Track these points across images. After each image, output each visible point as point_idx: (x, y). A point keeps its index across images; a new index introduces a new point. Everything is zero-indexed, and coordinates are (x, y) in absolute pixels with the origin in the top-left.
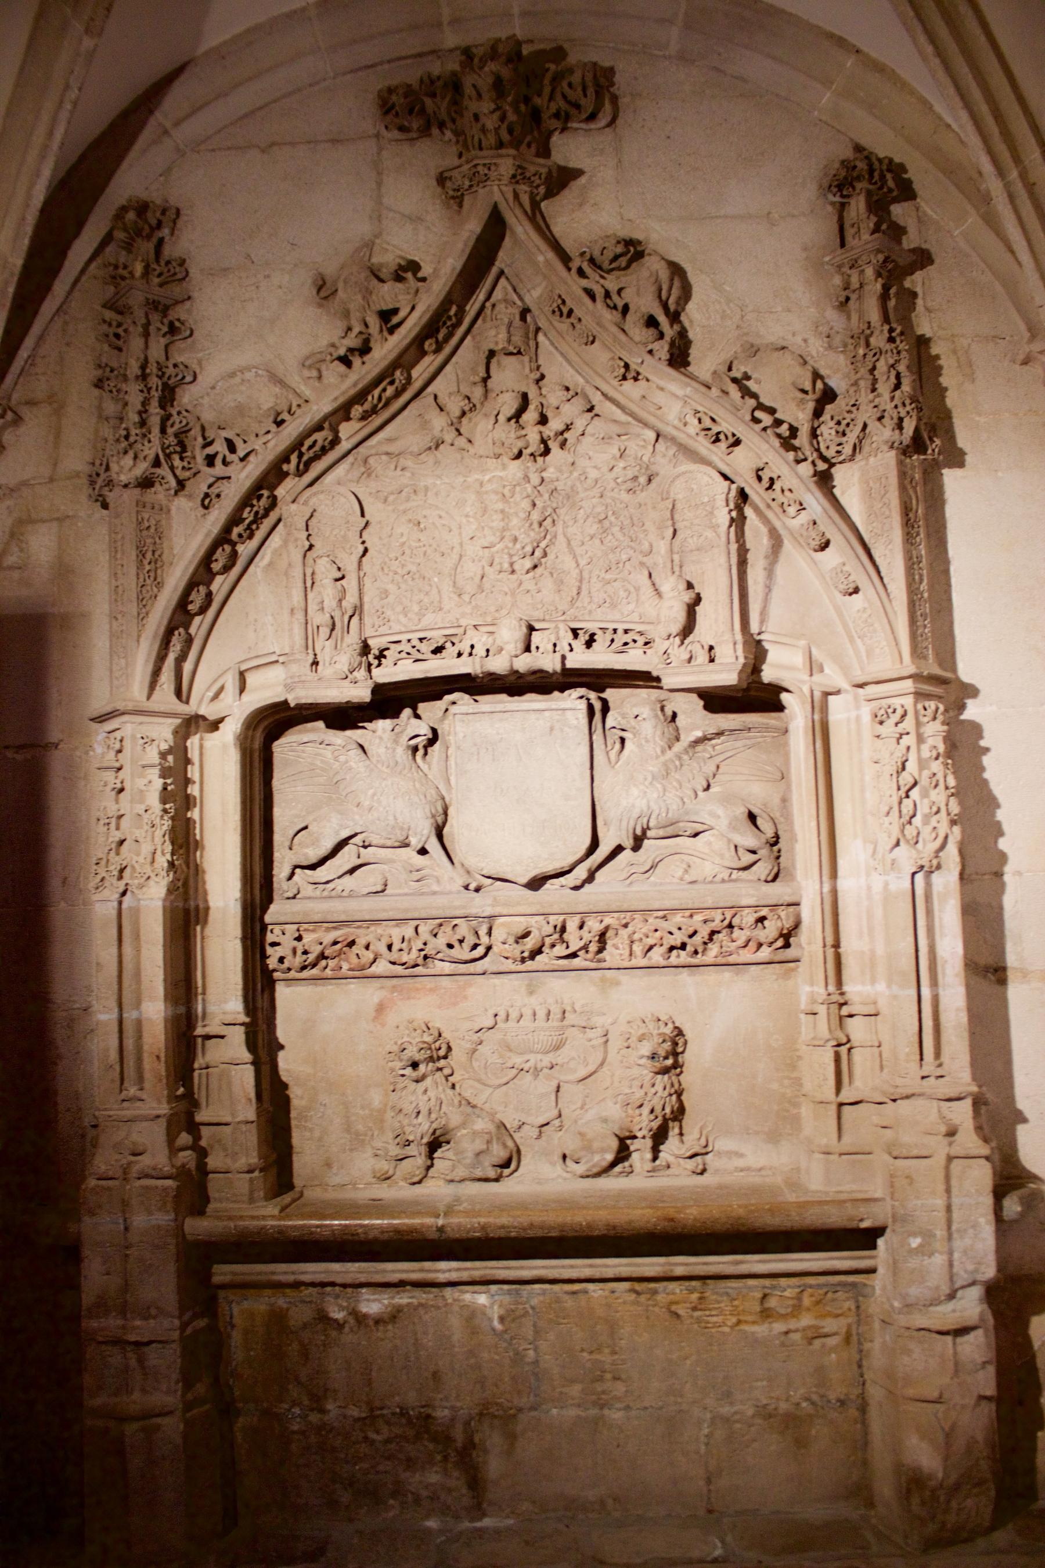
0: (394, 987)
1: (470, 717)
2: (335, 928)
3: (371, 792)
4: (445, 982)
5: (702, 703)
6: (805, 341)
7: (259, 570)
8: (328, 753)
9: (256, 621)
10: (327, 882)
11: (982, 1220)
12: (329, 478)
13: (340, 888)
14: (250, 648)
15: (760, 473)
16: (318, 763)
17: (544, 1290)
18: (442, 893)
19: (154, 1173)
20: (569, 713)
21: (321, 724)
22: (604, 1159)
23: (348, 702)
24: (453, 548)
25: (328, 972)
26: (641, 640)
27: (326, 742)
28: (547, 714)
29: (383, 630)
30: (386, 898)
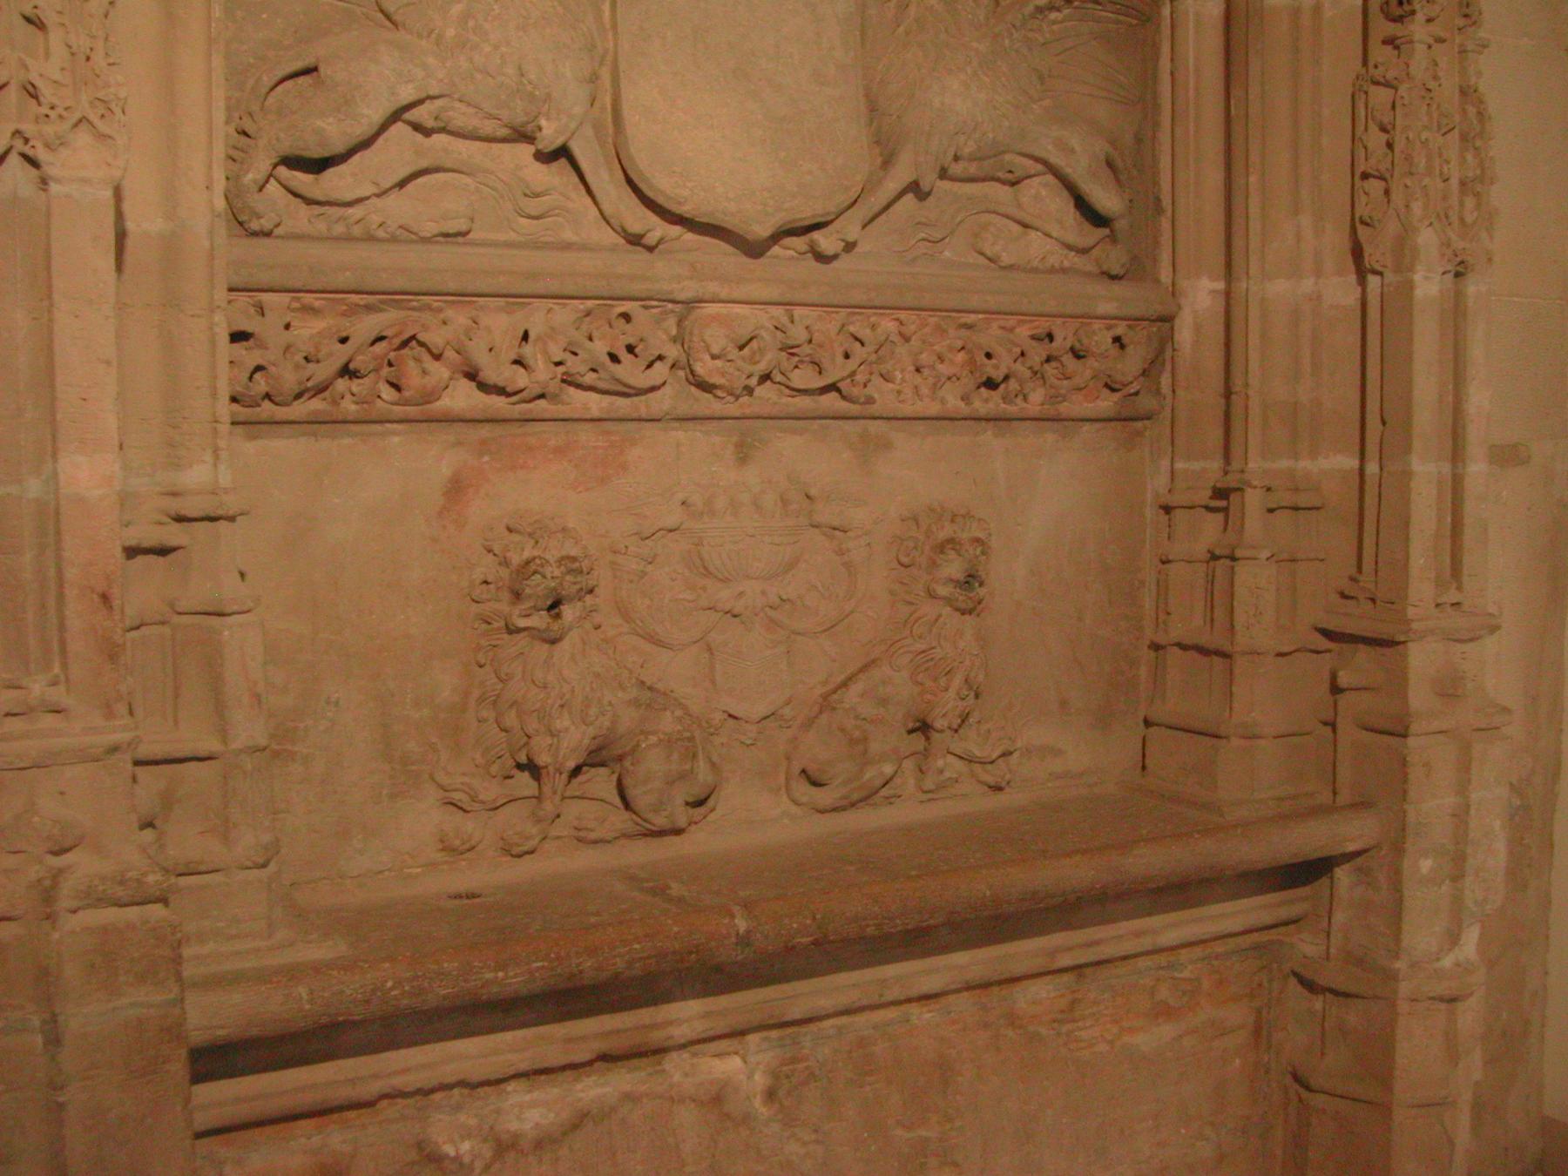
0: (483, 442)
2: (369, 308)
4: (586, 436)
10: (349, 204)
11: (1497, 824)
13: (376, 219)
17: (840, 1029)
18: (583, 247)
19: (120, 892)
22: (882, 773)
25: (349, 407)
30: (469, 249)
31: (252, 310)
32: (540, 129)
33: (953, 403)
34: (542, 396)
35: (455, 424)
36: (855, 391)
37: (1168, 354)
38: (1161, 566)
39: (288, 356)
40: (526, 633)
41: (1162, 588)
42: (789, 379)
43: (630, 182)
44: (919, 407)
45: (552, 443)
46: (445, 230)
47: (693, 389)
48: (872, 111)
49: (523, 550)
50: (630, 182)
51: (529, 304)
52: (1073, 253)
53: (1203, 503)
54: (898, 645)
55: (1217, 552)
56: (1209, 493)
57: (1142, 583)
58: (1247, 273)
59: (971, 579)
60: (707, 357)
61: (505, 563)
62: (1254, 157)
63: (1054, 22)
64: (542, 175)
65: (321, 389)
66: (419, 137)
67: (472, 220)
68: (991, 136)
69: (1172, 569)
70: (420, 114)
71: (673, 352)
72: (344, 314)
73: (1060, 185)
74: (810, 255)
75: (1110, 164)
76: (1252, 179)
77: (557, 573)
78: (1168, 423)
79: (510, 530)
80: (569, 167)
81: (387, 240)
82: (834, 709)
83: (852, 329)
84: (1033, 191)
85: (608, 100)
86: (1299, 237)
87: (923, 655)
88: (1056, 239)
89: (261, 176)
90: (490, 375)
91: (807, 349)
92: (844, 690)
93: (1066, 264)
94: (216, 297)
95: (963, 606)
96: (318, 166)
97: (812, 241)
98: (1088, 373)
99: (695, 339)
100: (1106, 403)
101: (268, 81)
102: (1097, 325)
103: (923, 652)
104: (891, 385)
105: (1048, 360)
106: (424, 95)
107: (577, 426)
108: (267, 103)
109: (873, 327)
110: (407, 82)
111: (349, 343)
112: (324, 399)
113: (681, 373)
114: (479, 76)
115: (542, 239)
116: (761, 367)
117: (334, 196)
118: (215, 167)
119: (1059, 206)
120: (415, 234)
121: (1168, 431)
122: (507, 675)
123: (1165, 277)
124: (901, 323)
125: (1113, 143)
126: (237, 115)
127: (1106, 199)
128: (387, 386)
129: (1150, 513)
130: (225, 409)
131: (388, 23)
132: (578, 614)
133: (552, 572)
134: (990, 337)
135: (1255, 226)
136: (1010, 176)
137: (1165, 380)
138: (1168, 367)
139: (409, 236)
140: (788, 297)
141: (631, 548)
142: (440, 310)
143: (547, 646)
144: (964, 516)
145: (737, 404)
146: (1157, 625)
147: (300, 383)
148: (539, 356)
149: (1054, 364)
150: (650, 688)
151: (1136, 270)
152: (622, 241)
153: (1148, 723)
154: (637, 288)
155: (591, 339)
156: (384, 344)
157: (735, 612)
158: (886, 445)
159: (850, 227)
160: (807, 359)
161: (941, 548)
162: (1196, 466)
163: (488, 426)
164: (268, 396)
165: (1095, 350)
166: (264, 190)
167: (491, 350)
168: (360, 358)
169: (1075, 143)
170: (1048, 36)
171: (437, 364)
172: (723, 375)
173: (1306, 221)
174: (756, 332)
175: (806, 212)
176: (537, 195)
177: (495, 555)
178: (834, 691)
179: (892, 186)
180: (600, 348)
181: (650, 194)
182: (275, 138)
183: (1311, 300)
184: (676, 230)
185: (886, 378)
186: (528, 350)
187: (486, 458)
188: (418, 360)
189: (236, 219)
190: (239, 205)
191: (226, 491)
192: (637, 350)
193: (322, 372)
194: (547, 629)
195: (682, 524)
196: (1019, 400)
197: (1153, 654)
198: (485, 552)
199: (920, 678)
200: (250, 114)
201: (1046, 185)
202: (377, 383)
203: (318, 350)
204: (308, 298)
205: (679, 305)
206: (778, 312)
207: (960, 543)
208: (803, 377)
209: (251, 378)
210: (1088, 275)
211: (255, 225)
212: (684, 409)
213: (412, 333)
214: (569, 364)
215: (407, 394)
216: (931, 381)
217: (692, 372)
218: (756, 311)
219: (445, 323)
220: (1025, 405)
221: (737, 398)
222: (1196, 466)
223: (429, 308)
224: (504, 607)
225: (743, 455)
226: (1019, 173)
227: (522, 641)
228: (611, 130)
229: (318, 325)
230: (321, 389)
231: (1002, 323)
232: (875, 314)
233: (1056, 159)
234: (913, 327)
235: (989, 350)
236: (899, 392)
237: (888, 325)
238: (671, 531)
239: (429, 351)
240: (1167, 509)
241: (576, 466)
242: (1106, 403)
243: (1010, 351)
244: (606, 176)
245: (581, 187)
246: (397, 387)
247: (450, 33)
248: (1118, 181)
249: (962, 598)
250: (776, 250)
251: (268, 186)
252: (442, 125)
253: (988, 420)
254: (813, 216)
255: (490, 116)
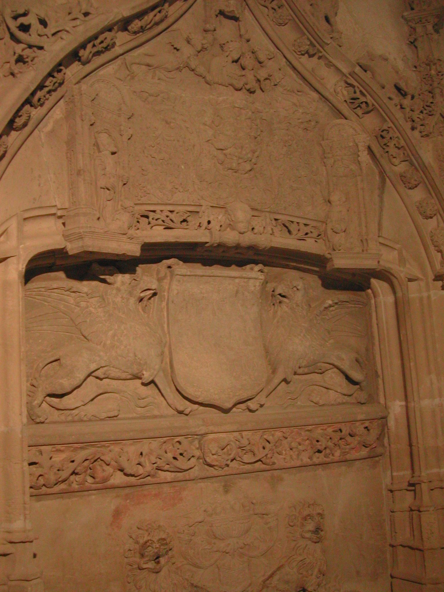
0: (127, 495)
1: (186, 278)
3: (110, 333)
4: (166, 489)
5: (320, 282)
6: (395, 59)
7: (43, 136)
8: (71, 299)
9: (40, 176)
12: (102, 72)
13: (83, 413)
14: (35, 199)
15: (387, 132)
16: (62, 307)
18: (162, 416)
20: (251, 281)
21: (61, 274)
23: (124, 254)
24: (194, 146)
25: (75, 486)
26: (315, 234)
27: (74, 290)
28: (237, 281)
29: (144, 200)
30: (119, 422)
31: (38, 454)
32: (143, 375)
33: (306, 460)
34: (149, 476)
35: (116, 489)
36: (268, 461)
37: (386, 430)
38: (391, 513)
39: (51, 469)
40: (146, 569)
41: (392, 523)
42: (242, 459)
43: (177, 390)
44: (293, 463)
45: (154, 492)
46: (109, 416)
47: (206, 466)
48: (267, 352)
49: (144, 537)
50: (177, 390)
51: (141, 441)
52: (346, 397)
53: (405, 488)
54: (291, 558)
55: (413, 508)
56: (407, 484)
57: (384, 520)
58: (414, 400)
59: (318, 530)
60: (211, 455)
61: (137, 543)
62: (412, 356)
63: (332, 311)
64: (144, 391)
65: (63, 481)
66: (98, 381)
67: (119, 411)
68: (312, 358)
69: (396, 514)
70: (99, 373)
71: (197, 453)
72: (72, 451)
73: (340, 372)
74: (247, 410)
75: (357, 360)
76: (412, 364)
77: (157, 546)
78: (388, 457)
79: (138, 528)
80: (155, 387)
81: (87, 421)
82: (268, 587)
83: (265, 437)
84: (329, 375)
85: (168, 360)
86: (432, 383)
87: (301, 562)
88: (339, 393)
89: (39, 402)
90: (128, 471)
91: (248, 448)
92: (271, 578)
93: (344, 401)
94: (24, 456)
95: (316, 541)
96: (61, 396)
97: (248, 405)
98: (356, 442)
99: (206, 448)
100: (364, 452)
101: (41, 365)
102: (358, 424)
103: (301, 561)
104: (281, 456)
105: (341, 439)
106: (100, 366)
107: (162, 485)
108: (41, 373)
109: (273, 435)
110: (93, 363)
111: (75, 462)
112: (66, 484)
113: (201, 461)
114: (120, 358)
115: (146, 415)
116: (231, 457)
117: (69, 407)
118: (23, 406)
119: (340, 379)
120: (98, 418)
121: (389, 459)
122: (139, 587)
123: (382, 401)
124: (284, 433)
125: (357, 353)
126: (30, 379)
127: (356, 376)
128: (89, 477)
129: (384, 492)
130: (28, 491)
131: (85, 340)
132: (166, 560)
133: (156, 546)
134: (318, 432)
135: (414, 381)
136: (320, 371)
137: (386, 441)
138: (386, 435)
139: (95, 419)
140: (240, 429)
141: (186, 531)
142: (109, 446)
143: (155, 574)
144: (313, 505)
145: (223, 470)
146: (392, 537)
147: (56, 480)
148: (147, 461)
149: (343, 440)
150: (196, 586)
151: (372, 399)
152: (176, 413)
153: (392, 577)
154: (183, 432)
155: (166, 453)
156: (87, 462)
157: (227, 551)
158: (281, 479)
159: (262, 399)
160: (249, 451)
161: (305, 518)
162: (402, 473)
163: (128, 489)
164: (44, 485)
165: (358, 433)
166: (41, 406)
167: (128, 460)
168: (79, 468)
169: (344, 356)
170: (330, 316)
171: (108, 467)
172: (217, 461)
173: (433, 376)
174: (229, 443)
175: (245, 395)
176: (143, 399)
177: (133, 539)
178: (268, 579)
179: (276, 381)
180: (170, 455)
181: (185, 395)
182: (45, 387)
183: (439, 406)
184: (196, 406)
185: (279, 453)
186: (142, 460)
187: (128, 501)
188: (101, 466)
189: (31, 418)
190: (32, 413)
191: (29, 531)
192: (184, 455)
193: (64, 475)
194: (154, 569)
195: (204, 519)
196: (331, 456)
197: (391, 548)
198: (130, 538)
199: (301, 571)
200: (35, 378)
201: (334, 372)
202: (86, 476)
203: (63, 466)
204: (59, 447)
205: (199, 436)
206: (236, 434)
207: (313, 517)
208: (248, 458)
209: (37, 479)
210: (352, 404)
211: (38, 420)
212: (203, 475)
213: (98, 457)
214: (158, 463)
215: (97, 480)
216: (297, 453)
217: (205, 460)
218: (228, 435)
219: (110, 451)
220: (333, 457)
221: (223, 468)
222: (402, 473)
223: (104, 446)
224: (137, 559)
225: (227, 489)
226: (323, 370)
227: (145, 573)
228: (170, 371)
229: (63, 456)
230: (63, 481)
231: (322, 428)
232: (273, 431)
233: (337, 363)
234: (288, 434)
235: (318, 439)
236: (285, 459)
237: (278, 434)
238: (200, 522)
239: (105, 463)
240: (391, 491)
241: (163, 501)
242: (364, 452)
243: (325, 438)
244: (168, 390)
245: (160, 394)
246: (94, 478)
247: (108, 342)
248: (361, 367)
249: (314, 537)
250: (234, 409)
251: (42, 404)
252: (107, 376)
253: (319, 465)
254: (248, 397)
255: (124, 372)
